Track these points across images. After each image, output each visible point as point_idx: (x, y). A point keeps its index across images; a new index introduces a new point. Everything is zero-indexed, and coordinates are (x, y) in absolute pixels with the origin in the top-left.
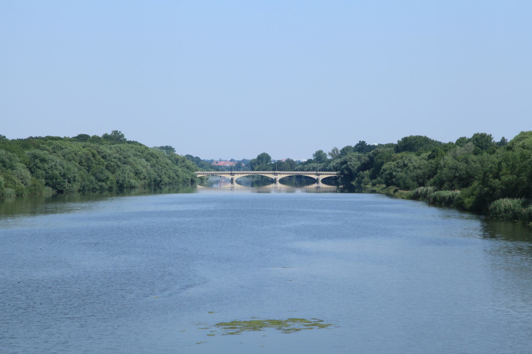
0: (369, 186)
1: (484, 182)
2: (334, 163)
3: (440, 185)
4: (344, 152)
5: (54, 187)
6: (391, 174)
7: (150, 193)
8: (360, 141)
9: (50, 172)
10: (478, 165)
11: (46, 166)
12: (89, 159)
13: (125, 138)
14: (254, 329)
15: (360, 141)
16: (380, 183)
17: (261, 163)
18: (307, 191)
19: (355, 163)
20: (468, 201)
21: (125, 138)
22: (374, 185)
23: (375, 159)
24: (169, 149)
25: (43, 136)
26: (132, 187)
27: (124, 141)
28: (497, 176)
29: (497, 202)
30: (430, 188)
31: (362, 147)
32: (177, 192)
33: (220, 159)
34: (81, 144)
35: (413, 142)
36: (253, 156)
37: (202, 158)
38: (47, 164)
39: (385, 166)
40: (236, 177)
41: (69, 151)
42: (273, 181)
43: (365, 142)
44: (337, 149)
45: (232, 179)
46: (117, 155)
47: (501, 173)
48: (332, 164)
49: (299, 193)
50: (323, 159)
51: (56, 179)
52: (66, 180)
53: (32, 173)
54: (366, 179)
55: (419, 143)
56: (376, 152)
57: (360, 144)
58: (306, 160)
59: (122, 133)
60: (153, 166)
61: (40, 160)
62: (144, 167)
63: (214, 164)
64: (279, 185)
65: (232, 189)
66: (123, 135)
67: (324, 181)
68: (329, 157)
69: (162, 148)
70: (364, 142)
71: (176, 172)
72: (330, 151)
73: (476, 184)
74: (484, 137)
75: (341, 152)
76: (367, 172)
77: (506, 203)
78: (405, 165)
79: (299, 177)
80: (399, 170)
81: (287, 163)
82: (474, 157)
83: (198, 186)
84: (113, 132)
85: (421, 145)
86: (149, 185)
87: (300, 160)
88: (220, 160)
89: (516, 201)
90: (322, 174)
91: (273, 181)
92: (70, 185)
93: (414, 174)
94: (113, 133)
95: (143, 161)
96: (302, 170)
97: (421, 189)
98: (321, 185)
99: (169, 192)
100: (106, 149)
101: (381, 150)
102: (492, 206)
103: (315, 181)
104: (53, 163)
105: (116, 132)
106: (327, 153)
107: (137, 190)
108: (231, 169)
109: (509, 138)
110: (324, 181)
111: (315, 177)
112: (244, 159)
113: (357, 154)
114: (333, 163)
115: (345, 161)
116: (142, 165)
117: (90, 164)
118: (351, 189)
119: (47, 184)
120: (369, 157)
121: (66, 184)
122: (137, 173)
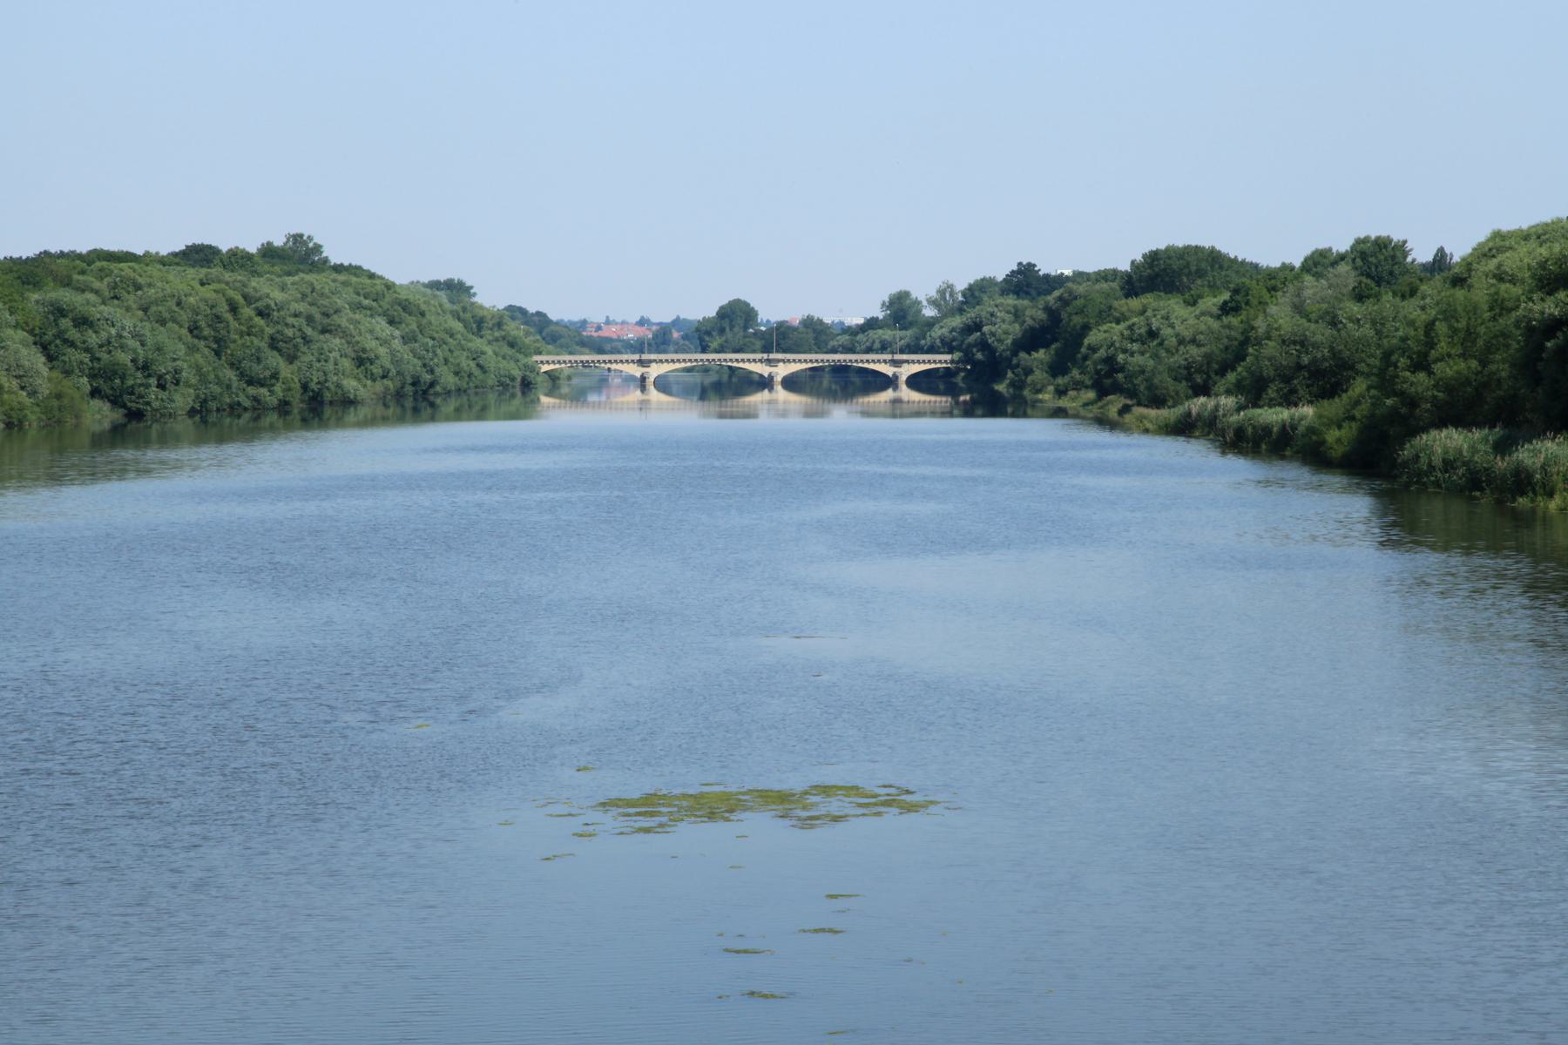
0: (1047, 396)
1: (1385, 381)
3: (1254, 392)
5: (115, 402)
6: (1110, 360)
7: (401, 420)
8: (1020, 264)
9: (105, 356)
10: (1367, 331)
11: (93, 339)
12: (218, 318)
13: (324, 255)
14: (712, 816)
16: (1078, 386)
17: (728, 329)
18: (867, 414)
19: (1004, 329)
20: (1338, 438)
21: (324, 255)
22: (1060, 392)
23: (1064, 315)
24: (456, 289)
25: (83, 248)
26: (348, 402)
27: (323, 265)
28: (1421, 364)
29: (1425, 439)
30: (1228, 402)
31: (1025, 281)
32: (481, 415)
33: (608, 317)
34: (194, 273)
35: (1176, 264)
36: (706, 309)
37: (553, 316)
38: (96, 332)
39: (1093, 338)
40: (654, 371)
41: (161, 295)
42: (765, 383)
43: (1035, 265)
44: (951, 287)
45: (643, 379)
46: (302, 307)
47: (1433, 354)
48: (937, 332)
49: (842, 418)
50: (910, 318)
51: (123, 378)
52: (153, 381)
53: (50, 358)
54: (1039, 375)
55: (1193, 268)
56: (1066, 295)
57: (1019, 272)
58: (861, 321)
59: (317, 240)
60: (406, 339)
61: (74, 320)
62: (385, 342)
63: (589, 332)
64: (781, 394)
65: (643, 406)
66: (321, 246)
67: (915, 382)
68: (929, 312)
69: (435, 285)
70: (1031, 266)
71: (476, 356)
72: (933, 293)
73: (1359, 386)
75: (964, 295)
76: (1041, 354)
77: (1447, 441)
78: (1152, 334)
79: (840, 370)
80: (1135, 347)
81: (804, 330)
82: (1355, 309)
83: (544, 400)
85: (1201, 273)
86: (399, 395)
87: (842, 319)
89: (1477, 434)
91: (765, 383)
92: (163, 395)
93: (1178, 360)
94: (288, 240)
95: (381, 325)
96: (851, 350)
97: (1198, 404)
98: (907, 394)
99: (458, 415)
100: (269, 288)
101: (1081, 289)
102: (1407, 453)
103: (888, 382)
104: (113, 331)
105: (297, 238)
106: (922, 298)
107: (363, 412)
108: (639, 347)
109: (1459, 251)
110: (915, 382)
111: (888, 370)
112: (678, 317)
113: (1011, 301)
114: (942, 327)
115: (975, 323)
116: (378, 335)
118: (993, 407)
119: (95, 393)
120: (1047, 309)
121: (153, 393)
122: (362, 361)
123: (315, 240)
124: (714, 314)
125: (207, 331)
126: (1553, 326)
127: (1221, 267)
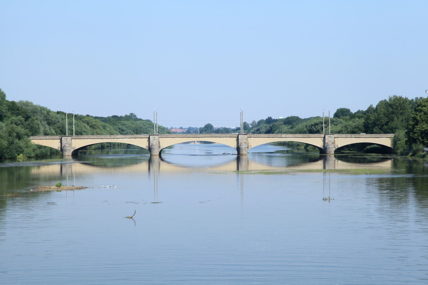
2: (253, 130)
4: (259, 123)
8: (268, 117)
12: (137, 129)
13: (137, 117)
15: (268, 117)
17: (207, 130)
21: (137, 117)
23: (273, 128)
27: (137, 119)
33: (172, 127)
38: (124, 132)
41: (129, 126)
43: (271, 117)
44: (255, 121)
50: (247, 128)
55: (294, 120)
57: (268, 119)
58: (235, 128)
59: (135, 114)
70: (271, 118)
72: (251, 123)
74: (406, 101)
75: (258, 123)
85: (295, 121)
87: (230, 127)
88: (172, 128)
94: (130, 114)
104: (127, 132)
105: (132, 114)
106: (249, 123)
112: (190, 127)
114: (253, 130)
115: (258, 129)
120: (270, 127)
124: (204, 127)
125: (135, 132)
126: (427, 130)
127: (299, 120)
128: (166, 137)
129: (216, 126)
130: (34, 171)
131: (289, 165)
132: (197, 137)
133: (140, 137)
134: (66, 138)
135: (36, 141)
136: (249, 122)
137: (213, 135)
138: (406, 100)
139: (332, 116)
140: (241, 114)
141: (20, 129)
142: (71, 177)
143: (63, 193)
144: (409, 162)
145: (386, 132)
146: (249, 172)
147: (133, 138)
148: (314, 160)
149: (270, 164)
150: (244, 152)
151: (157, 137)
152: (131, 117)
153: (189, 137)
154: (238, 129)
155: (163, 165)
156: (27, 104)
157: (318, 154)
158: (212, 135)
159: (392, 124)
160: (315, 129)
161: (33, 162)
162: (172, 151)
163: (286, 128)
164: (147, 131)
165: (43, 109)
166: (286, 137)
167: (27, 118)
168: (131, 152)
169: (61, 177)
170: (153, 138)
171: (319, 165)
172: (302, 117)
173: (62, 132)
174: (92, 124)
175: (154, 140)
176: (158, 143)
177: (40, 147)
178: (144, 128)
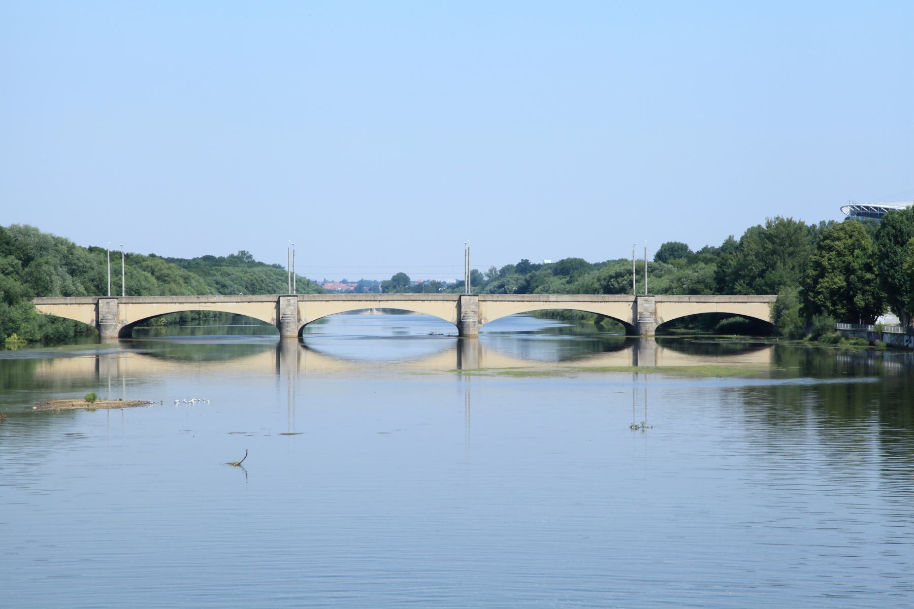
2: (491, 287)
4: (504, 272)
8: (522, 260)
12: (253, 284)
15: (522, 260)
17: (397, 286)
27: (253, 264)
33: (325, 279)
43: (528, 261)
44: (495, 269)
55: (574, 266)
56: (532, 275)
57: (522, 263)
58: (454, 282)
61: (221, 285)
66: (252, 256)
70: (527, 261)
72: (487, 271)
74: (801, 229)
81: (432, 287)
84: (239, 252)
85: (577, 269)
87: (445, 280)
88: (325, 281)
90: (796, 565)
105: (243, 253)
106: (483, 273)
112: (362, 279)
114: (490, 286)
115: (502, 284)
117: (255, 289)
120: (526, 280)
123: (249, 253)
125: (250, 289)
127: (584, 266)
128: (313, 299)
129: (415, 278)
130: (41, 370)
131: (563, 359)
132: (376, 301)
133: (259, 301)
134: (107, 303)
135: (46, 307)
136: (483, 270)
137: (409, 295)
138: (800, 226)
139: (651, 258)
140: (467, 253)
141: (15, 285)
142: (117, 381)
143: (101, 413)
144: (807, 352)
145: (760, 291)
146: (481, 371)
147: (246, 302)
148: (613, 347)
149: (525, 356)
150: (471, 331)
151: (294, 299)
152: (242, 260)
153: (359, 301)
154: (461, 284)
155: (306, 357)
156: (26, 232)
157: (620, 335)
158: (406, 296)
159: (772, 276)
160: (616, 285)
161: (39, 349)
162: (327, 329)
163: (557, 282)
164: (275, 288)
165: (59, 242)
166: (559, 300)
167: (27, 260)
168: (242, 332)
169: (97, 381)
170: (286, 303)
171: (624, 358)
172: (591, 260)
173: (99, 290)
174: (161, 274)
175: (289, 305)
176: (296, 313)
177: (53, 320)
178: (268, 280)
